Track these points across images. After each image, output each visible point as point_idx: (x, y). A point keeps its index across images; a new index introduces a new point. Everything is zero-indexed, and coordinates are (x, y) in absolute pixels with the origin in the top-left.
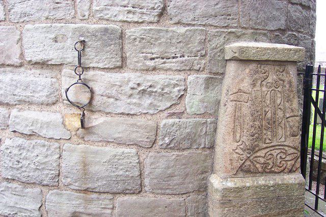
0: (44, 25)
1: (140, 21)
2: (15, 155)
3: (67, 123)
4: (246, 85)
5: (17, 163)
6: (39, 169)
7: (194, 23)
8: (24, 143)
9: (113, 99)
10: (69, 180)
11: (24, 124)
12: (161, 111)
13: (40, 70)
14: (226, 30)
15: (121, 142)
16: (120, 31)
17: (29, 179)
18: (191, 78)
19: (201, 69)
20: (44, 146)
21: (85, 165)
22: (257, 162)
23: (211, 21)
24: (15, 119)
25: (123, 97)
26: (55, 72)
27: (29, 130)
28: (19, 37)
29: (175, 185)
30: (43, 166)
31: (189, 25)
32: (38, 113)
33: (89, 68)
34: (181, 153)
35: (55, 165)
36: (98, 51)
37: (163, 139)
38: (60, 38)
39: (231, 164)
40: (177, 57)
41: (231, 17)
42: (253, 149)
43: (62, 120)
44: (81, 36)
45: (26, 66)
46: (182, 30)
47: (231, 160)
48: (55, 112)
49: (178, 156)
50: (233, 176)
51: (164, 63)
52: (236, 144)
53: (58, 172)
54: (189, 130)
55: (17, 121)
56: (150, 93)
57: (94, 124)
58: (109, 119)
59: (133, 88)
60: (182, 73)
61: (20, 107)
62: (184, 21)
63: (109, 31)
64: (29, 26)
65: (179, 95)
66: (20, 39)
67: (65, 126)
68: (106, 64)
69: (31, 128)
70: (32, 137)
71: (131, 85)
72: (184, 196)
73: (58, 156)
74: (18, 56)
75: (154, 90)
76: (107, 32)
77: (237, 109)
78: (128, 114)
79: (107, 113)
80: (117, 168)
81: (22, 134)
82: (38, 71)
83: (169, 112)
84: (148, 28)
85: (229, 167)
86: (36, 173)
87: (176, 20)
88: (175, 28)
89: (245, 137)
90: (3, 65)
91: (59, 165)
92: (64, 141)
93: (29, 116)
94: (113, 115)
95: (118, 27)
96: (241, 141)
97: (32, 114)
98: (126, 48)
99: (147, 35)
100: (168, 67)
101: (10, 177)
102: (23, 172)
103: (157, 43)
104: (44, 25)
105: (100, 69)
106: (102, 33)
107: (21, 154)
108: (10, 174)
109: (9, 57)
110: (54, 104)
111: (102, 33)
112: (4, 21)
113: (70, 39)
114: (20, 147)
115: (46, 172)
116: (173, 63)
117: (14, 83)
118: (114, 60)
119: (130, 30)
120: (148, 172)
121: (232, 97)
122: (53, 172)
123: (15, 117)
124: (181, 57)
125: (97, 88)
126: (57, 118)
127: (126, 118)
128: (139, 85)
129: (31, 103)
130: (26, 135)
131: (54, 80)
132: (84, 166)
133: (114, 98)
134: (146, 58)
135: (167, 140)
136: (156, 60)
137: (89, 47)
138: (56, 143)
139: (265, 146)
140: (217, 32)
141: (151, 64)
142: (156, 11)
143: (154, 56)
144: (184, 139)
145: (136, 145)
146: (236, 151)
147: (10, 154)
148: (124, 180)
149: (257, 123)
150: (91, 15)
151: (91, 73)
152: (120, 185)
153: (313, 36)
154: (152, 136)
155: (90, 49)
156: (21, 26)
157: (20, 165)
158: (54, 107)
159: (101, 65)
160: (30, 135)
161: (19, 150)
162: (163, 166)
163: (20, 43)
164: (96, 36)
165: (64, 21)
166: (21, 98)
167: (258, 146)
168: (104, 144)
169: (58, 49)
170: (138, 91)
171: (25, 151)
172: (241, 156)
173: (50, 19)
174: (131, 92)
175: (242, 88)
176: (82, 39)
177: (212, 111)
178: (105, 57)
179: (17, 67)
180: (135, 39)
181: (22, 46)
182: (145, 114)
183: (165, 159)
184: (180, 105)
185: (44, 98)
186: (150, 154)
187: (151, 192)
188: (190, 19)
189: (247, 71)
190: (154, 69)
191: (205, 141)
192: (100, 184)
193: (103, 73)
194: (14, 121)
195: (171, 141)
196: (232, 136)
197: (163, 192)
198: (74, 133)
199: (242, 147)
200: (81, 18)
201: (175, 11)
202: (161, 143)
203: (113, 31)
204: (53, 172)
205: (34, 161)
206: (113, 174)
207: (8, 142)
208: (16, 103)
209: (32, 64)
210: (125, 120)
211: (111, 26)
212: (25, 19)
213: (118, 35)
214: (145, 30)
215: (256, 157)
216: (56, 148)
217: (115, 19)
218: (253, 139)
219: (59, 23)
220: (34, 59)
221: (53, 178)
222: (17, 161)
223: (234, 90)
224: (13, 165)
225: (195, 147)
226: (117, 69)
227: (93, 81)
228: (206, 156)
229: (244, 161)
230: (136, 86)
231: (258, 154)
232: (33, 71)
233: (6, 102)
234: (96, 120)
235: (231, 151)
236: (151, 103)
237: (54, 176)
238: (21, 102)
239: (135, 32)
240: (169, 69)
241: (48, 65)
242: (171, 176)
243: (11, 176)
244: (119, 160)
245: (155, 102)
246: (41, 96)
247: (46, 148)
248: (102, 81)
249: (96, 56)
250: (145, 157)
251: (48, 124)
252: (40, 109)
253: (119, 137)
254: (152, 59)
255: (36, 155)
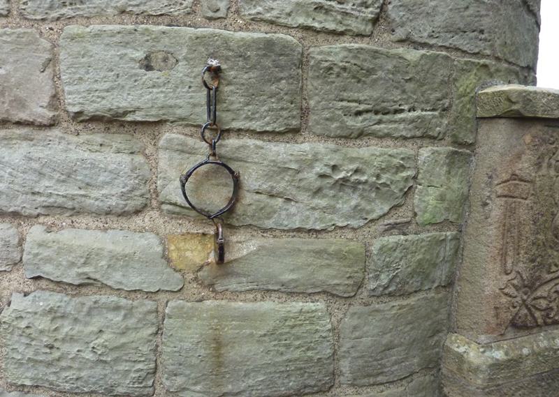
0: (117, 27)
1: (341, 29)
2: (42, 332)
3: (174, 255)
4: (526, 165)
5: (48, 351)
6: (105, 362)
7: (432, 42)
8: (63, 304)
9: (280, 200)
10: (180, 380)
11: (64, 260)
12: (372, 221)
13: (103, 135)
14: (477, 61)
15: (295, 290)
16: (300, 50)
17: (79, 383)
18: (426, 153)
19: (441, 136)
20: (117, 308)
21: (218, 344)
22: (537, 309)
23: (457, 41)
24: (40, 250)
25: (303, 197)
26: (142, 139)
27: (79, 275)
28: (47, 56)
29: (393, 365)
30: (115, 355)
31: (424, 45)
32: (100, 234)
33: (228, 131)
34: (405, 303)
35: (145, 349)
36: (252, 95)
37: (377, 277)
38: (157, 61)
39: (497, 316)
40: (402, 111)
41: (483, 36)
42: (530, 286)
43: (159, 249)
44: (212, 55)
45: (65, 125)
46: (413, 55)
47: (496, 308)
48: (142, 230)
49: (401, 307)
50: (499, 338)
51: (380, 122)
52: (506, 278)
53: (152, 365)
54: (420, 256)
55: (46, 253)
56: (355, 186)
57: (238, 255)
58: (269, 241)
59: (322, 176)
60: (409, 144)
61: (49, 220)
62: (416, 37)
63: (277, 49)
64: (73, 29)
65: (405, 187)
66: (52, 61)
67: (168, 260)
68: (268, 124)
69: (86, 269)
70: (84, 290)
71: (319, 168)
72: (404, 382)
73: (154, 329)
74: (45, 100)
75: (364, 178)
76: (272, 51)
77: (510, 212)
78: (310, 231)
79: (265, 230)
80: (288, 346)
81: (59, 283)
82: (98, 138)
83: (386, 222)
84: (356, 46)
85: (493, 321)
86: (99, 370)
87: (400, 33)
88: (400, 50)
89: (521, 265)
90: (3, 123)
91: (155, 350)
92: (168, 296)
93: (76, 243)
94: (277, 233)
95: (295, 41)
96: (514, 272)
97: (84, 237)
98: (310, 87)
99: (353, 61)
100: (386, 131)
101: (28, 383)
102: (63, 369)
103: (368, 80)
104: (117, 27)
105: (261, 134)
106: (260, 53)
107: (56, 329)
108: (29, 374)
109: (21, 103)
110: (137, 212)
111: (260, 53)
112: (6, 16)
113: (184, 63)
114: (53, 313)
115: (122, 367)
116: (395, 122)
117: (36, 165)
118: (285, 113)
119: (318, 50)
120: (349, 345)
121: (499, 190)
122: (140, 366)
123: (40, 245)
124: (409, 111)
125: (252, 179)
126: (150, 243)
127: (306, 238)
128: (334, 168)
129: (76, 212)
130: (70, 284)
131: (139, 159)
132: (217, 349)
133: (282, 197)
134: (347, 112)
135: (384, 279)
136: (365, 116)
137: (229, 84)
138: (147, 302)
139: (549, 277)
140: (466, 63)
141: (356, 123)
142: (371, 9)
143: (362, 107)
144: (411, 275)
145: (324, 292)
146: (506, 291)
147: (28, 331)
148: (301, 369)
149: (541, 237)
150: (233, 9)
151: (232, 142)
152: (293, 379)
153: (536, 74)
154: (357, 272)
155: (232, 88)
156: (51, 29)
157: (57, 354)
158: (138, 221)
159: (256, 125)
160: (80, 285)
161: (53, 319)
162: (376, 331)
163: (50, 70)
164: (246, 58)
165: (167, 20)
166: (52, 200)
167: (539, 278)
168: (259, 296)
169: (154, 86)
170: (331, 181)
171: (66, 323)
172: (514, 300)
173: (130, 13)
174: (318, 183)
175: (517, 172)
176: (214, 63)
177: (458, 214)
178: (266, 108)
179: (41, 126)
180: (330, 68)
181: (56, 76)
182: (342, 228)
183: (379, 316)
184: (404, 208)
185: (113, 202)
186: (352, 309)
187: (353, 385)
188: (425, 34)
189: (528, 138)
190: (361, 134)
191: (440, 274)
192: (251, 382)
193: (259, 143)
194: (37, 254)
195: (391, 281)
196: (498, 264)
197: (372, 380)
198: (190, 276)
199: (515, 282)
200: (210, 14)
201: (402, 13)
202: (372, 285)
203: (285, 49)
204: (140, 366)
205: (92, 345)
206: (279, 359)
207: (19, 303)
208: (39, 211)
209: (82, 122)
210: (304, 243)
211: (281, 35)
212: (64, 11)
213: (297, 56)
214: (350, 50)
215: (535, 299)
216: (150, 312)
217: (289, 21)
218: (534, 266)
219: (154, 23)
220: (90, 109)
221: (140, 380)
222: (46, 346)
223: (504, 175)
224: (36, 354)
225: (426, 288)
226: (290, 135)
227: (238, 160)
228: (440, 300)
229: (518, 308)
230: (329, 171)
231: (539, 293)
232: (84, 137)
233: (11, 210)
234: (244, 246)
235: (498, 291)
236: (356, 206)
237: (143, 374)
238: (50, 209)
239: (329, 54)
240: (388, 136)
241: (122, 124)
242: (389, 347)
243: (32, 379)
244: (293, 327)
245: (363, 204)
246: (109, 195)
247: (123, 312)
248: (259, 159)
249: (248, 104)
250: (341, 316)
251: (124, 261)
252: (101, 225)
253: (292, 280)
254: (359, 113)
255: (96, 329)
